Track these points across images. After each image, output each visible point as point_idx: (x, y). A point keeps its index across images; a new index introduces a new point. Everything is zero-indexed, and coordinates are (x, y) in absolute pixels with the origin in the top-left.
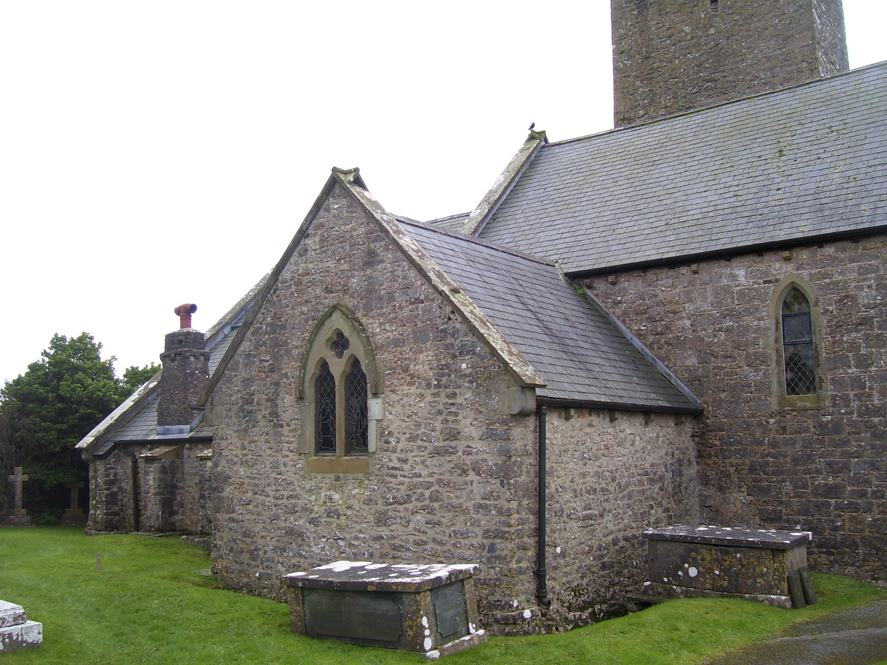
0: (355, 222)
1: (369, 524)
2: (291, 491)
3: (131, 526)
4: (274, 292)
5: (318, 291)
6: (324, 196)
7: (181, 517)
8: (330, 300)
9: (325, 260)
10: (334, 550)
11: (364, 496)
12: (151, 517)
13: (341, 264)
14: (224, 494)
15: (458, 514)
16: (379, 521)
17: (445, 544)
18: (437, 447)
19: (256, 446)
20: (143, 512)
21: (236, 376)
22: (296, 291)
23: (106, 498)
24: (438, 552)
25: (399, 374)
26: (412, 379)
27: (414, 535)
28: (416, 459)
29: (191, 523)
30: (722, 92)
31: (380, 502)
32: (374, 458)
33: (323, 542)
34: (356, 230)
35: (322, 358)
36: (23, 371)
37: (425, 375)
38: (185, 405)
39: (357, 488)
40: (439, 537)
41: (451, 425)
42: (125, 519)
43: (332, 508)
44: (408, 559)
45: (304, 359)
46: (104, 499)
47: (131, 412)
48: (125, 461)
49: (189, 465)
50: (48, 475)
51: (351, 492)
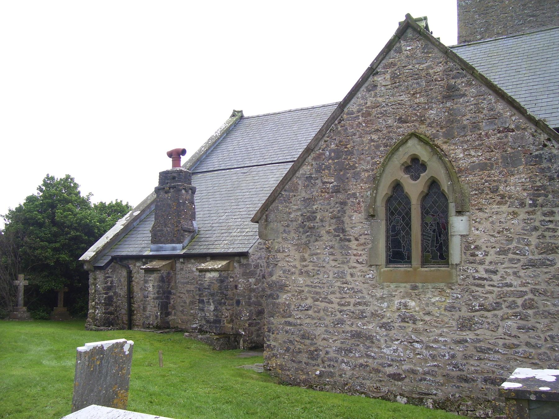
0: (431, 61)
1: (450, 329)
2: (358, 298)
3: (123, 323)
4: (339, 123)
5: (390, 121)
6: (397, 39)
7: (173, 317)
8: (405, 129)
9: (398, 94)
10: (408, 352)
11: (445, 303)
12: (150, 317)
13: (416, 98)
14: (279, 300)
15: (556, 320)
16: (463, 326)
17: (540, 348)
18: (532, 259)
19: (318, 259)
20: (135, 312)
21: (295, 196)
22: (364, 122)
23: (105, 301)
24: (532, 354)
25: (487, 194)
26: (502, 198)
27: (505, 339)
28: (508, 270)
29: (182, 322)
30: (541, 24)
31: (464, 309)
32: (458, 269)
33: (395, 344)
34: (433, 68)
35: (396, 180)
36: (22, 201)
37: (517, 195)
38: (178, 228)
39: (437, 297)
40: (533, 341)
41: (548, 240)
42: (118, 318)
43: (407, 314)
44: (496, 361)
45: (375, 180)
46: (103, 301)
47: (121, 234)
48: (120, 272)
49: (180, 277)
50: (43, 282)
51: (430, 299)
